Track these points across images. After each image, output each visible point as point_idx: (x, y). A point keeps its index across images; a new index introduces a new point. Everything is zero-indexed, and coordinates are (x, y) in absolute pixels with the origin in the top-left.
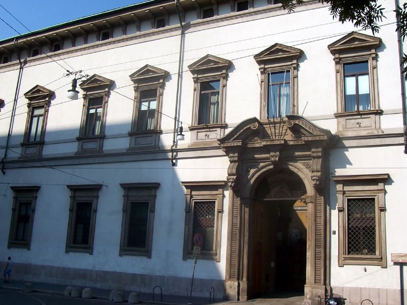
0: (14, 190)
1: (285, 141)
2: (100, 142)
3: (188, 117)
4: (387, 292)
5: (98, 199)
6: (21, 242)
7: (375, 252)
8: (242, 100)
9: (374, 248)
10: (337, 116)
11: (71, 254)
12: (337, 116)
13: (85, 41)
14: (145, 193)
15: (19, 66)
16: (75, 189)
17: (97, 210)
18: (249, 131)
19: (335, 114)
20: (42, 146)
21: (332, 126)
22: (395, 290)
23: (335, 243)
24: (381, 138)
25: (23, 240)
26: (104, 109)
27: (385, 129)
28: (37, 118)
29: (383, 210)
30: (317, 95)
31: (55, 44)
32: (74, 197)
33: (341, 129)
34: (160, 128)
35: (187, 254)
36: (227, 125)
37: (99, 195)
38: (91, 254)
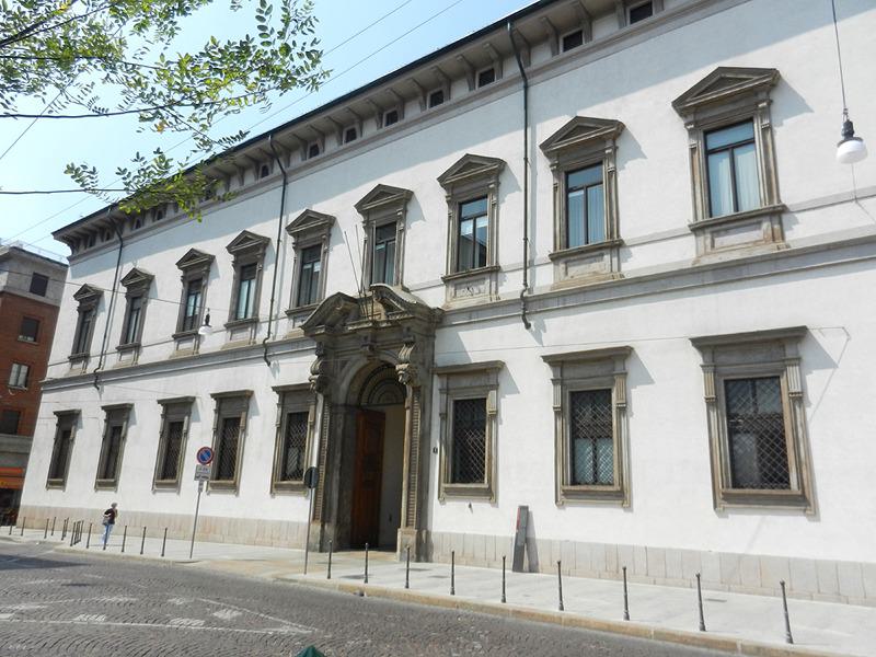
0: (550, 363)
1: (374, 322)
2: (17, 380)
3: (115, 339)
4: (837, 569)
5: (625, 378)
6: (592, 488)
7: (788, 482)
8: (344, 273)
9: (787, 475)
10: (697, 230)
11: (99, 492)
12: (697, 230)
13: (470, 85)
14: (482, 381)
15: (119, 245)
17: (497, 411)
19: (690, 226)
20: (494, 275)
21: (436, 298)
22: (298, 525)
23: (437, 466)
24: (493, 312)
25: (596, 482)
26: (323, 264)
27: (792, 241)
28: (472, 221)
29: (623, 410)
31: (346, 130)
32: (448, 389)
33: (449, 299)
34: (618, 236)
35: (100, 485)
36: (784, 206)
37: (801, 353)
38: (237, 495)
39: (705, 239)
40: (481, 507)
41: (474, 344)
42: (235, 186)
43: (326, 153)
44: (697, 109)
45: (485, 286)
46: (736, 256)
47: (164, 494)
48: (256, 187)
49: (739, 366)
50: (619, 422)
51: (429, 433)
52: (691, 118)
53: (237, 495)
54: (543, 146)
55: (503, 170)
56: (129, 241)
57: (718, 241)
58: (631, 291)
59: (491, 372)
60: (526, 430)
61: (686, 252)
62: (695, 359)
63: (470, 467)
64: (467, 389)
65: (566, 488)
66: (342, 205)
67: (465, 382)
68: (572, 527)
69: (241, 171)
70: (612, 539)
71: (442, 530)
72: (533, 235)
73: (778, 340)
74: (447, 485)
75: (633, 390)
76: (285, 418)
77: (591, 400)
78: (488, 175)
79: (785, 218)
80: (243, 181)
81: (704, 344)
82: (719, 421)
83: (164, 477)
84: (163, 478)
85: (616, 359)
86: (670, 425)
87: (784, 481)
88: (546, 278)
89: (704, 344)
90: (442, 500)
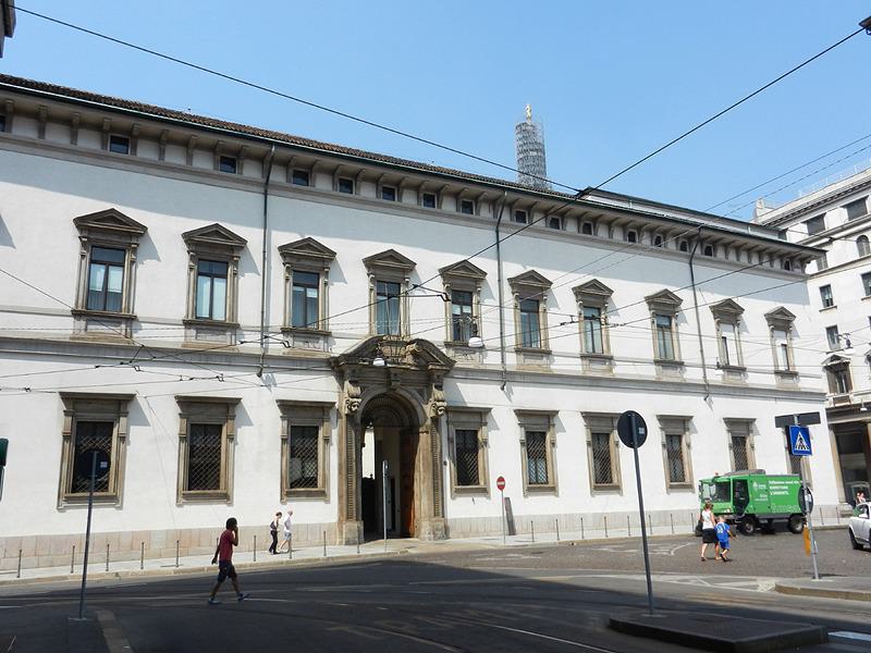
16: (73, 401)
18: (371, 348)
22: (81, 535)
30: (427, 317)
39: (586, 362)
40: (480, 499)
41: (472, 394)
42: (744, 259)
43: (239, 176)
44: (90, 230)
45: (321, 344)
46: (599, 375)
47: (676, 494)
48: (543, 232)
49: (202, 418)
50: (552, 452)
51: (432, 451)
52: (288, 260)
53: (121, 508)
54: (280, 248)
55: (242, 248)
56: (277, 192)
57: (90, 327)
58: (557, 380)
59: (482, 414)
60: (503, 451)
61: (176, 337)
62: (724, 427)
63: (468, 476)
64: (467, 423)
65: (68, 495)
66: (429, 263)
67: (464, 418)
68: (530, 508)
69: (772, 256)
70: (551, 512)
71: (454, 517)
72: (268, 307)
73: (323, 408)
74: (68, 495)
75: (239, 430)
76: (75, 425)
77: (537, 432)
78: (131, 235)
79: (134, 325)
80: (43, 134)
81: (67, 397)
82: (287, 447)
83: (75, 489)
84: (74, 491)
85: (121, 404)
86: (571, 451)
87: (475, 480)
88: (276, 347)
89: (67, 397)
90: (453, 498)
